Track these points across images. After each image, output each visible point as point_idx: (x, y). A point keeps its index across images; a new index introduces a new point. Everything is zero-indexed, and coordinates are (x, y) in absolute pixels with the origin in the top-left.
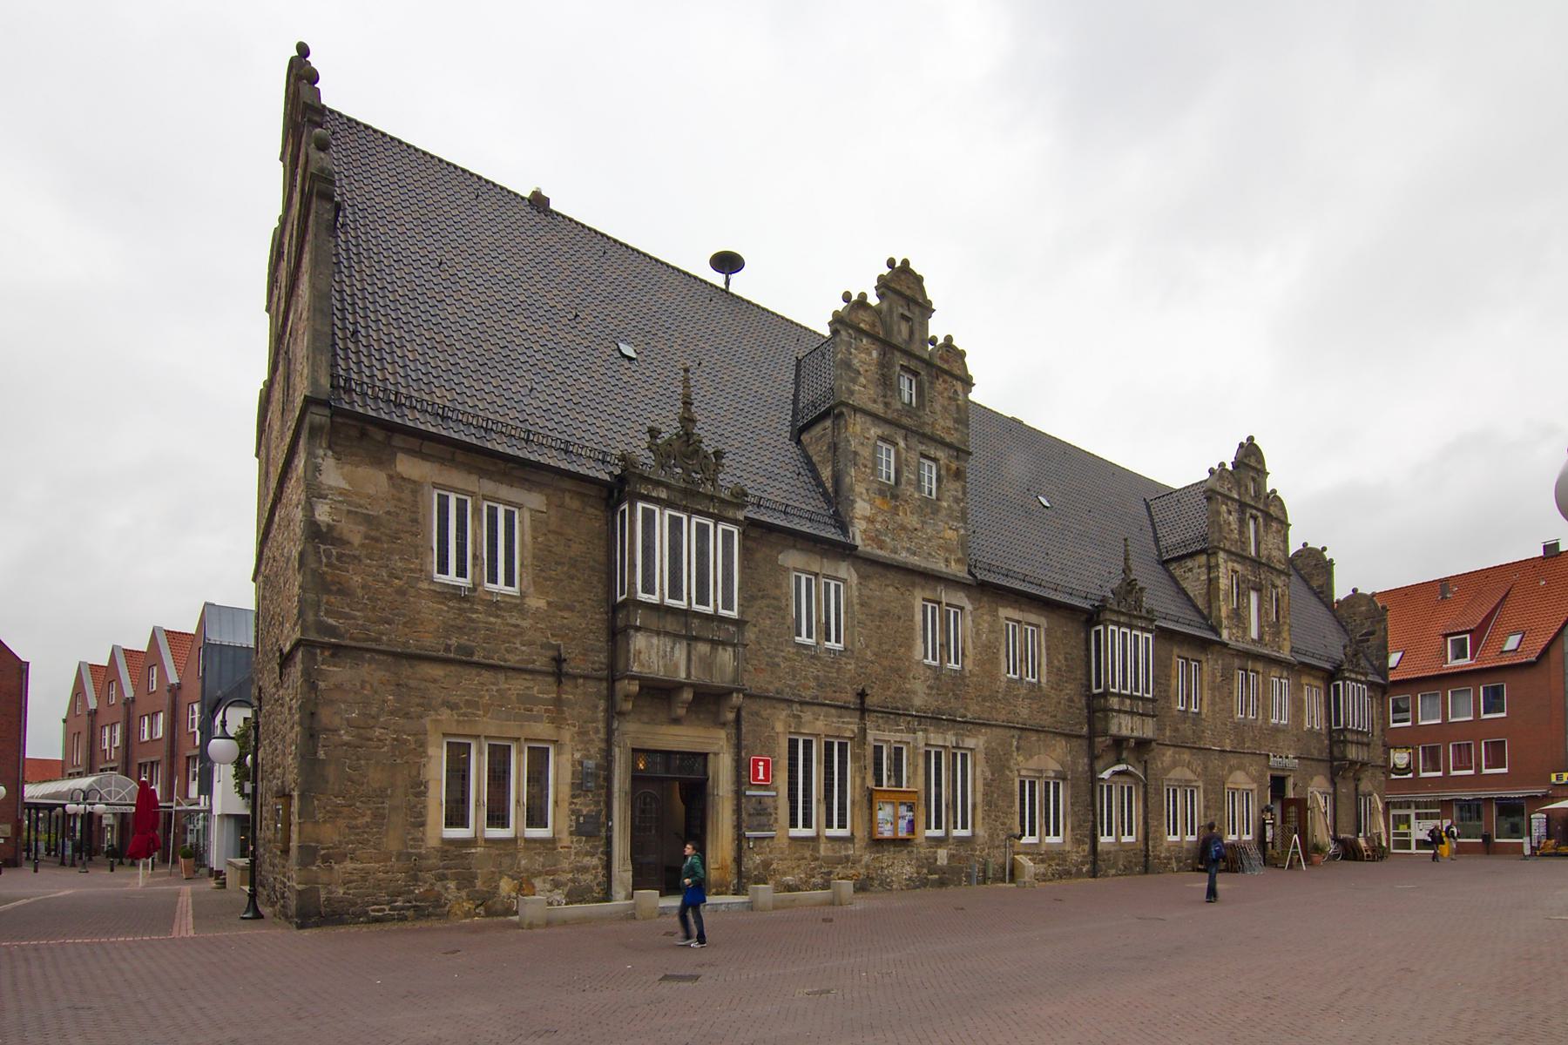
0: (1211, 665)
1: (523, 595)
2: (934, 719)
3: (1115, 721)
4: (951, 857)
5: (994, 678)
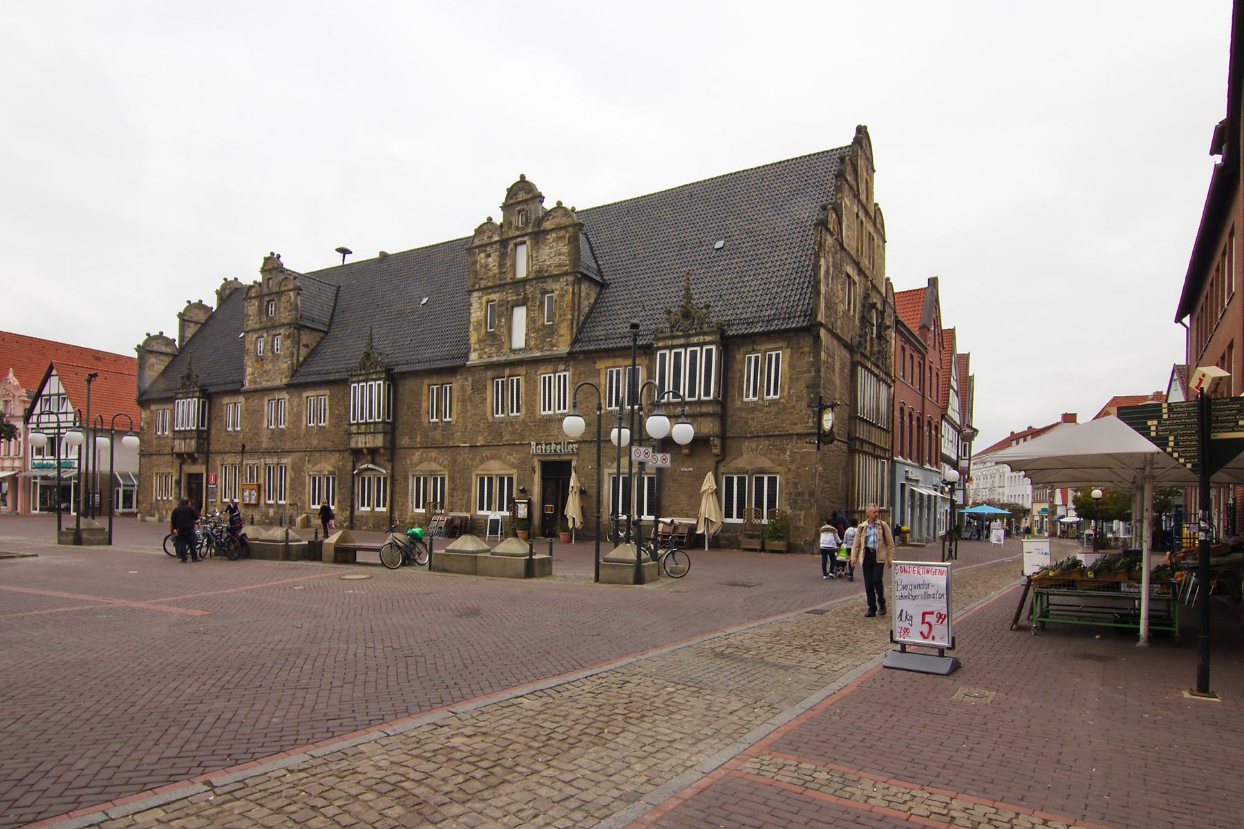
0: (457, 384)
2: (268, 453)
5: (299, 428)
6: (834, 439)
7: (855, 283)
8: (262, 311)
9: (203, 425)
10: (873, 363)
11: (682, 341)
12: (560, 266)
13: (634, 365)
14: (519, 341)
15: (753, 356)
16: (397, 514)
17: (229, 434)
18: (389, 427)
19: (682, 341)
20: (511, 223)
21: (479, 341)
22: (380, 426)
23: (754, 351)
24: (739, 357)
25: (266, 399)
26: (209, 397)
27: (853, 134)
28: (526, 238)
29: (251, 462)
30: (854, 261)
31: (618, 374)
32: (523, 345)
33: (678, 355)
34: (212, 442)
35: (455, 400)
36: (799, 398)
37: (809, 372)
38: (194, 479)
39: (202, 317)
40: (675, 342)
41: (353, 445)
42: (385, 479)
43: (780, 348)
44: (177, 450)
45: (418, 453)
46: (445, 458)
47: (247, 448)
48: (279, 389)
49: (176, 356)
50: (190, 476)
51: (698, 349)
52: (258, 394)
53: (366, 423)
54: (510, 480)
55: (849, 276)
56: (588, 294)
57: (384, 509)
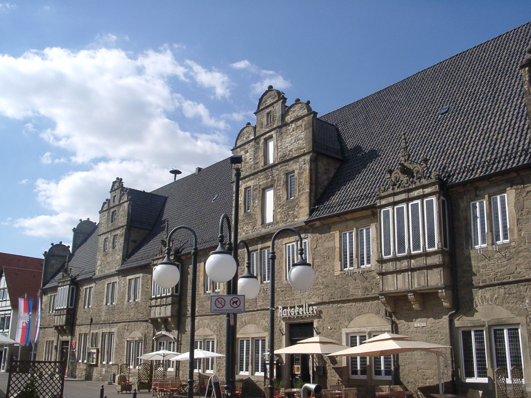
1: (510, 242)
3: (153, 312)
9: (71, 305)
11: (403, 196)
19: (403, 196)
22: (170, 299)
24: (462, 205)
28: (272, 133)
32: (272, 221)
40: (397, 198)
41: (152, 316)
47: (94, 321)
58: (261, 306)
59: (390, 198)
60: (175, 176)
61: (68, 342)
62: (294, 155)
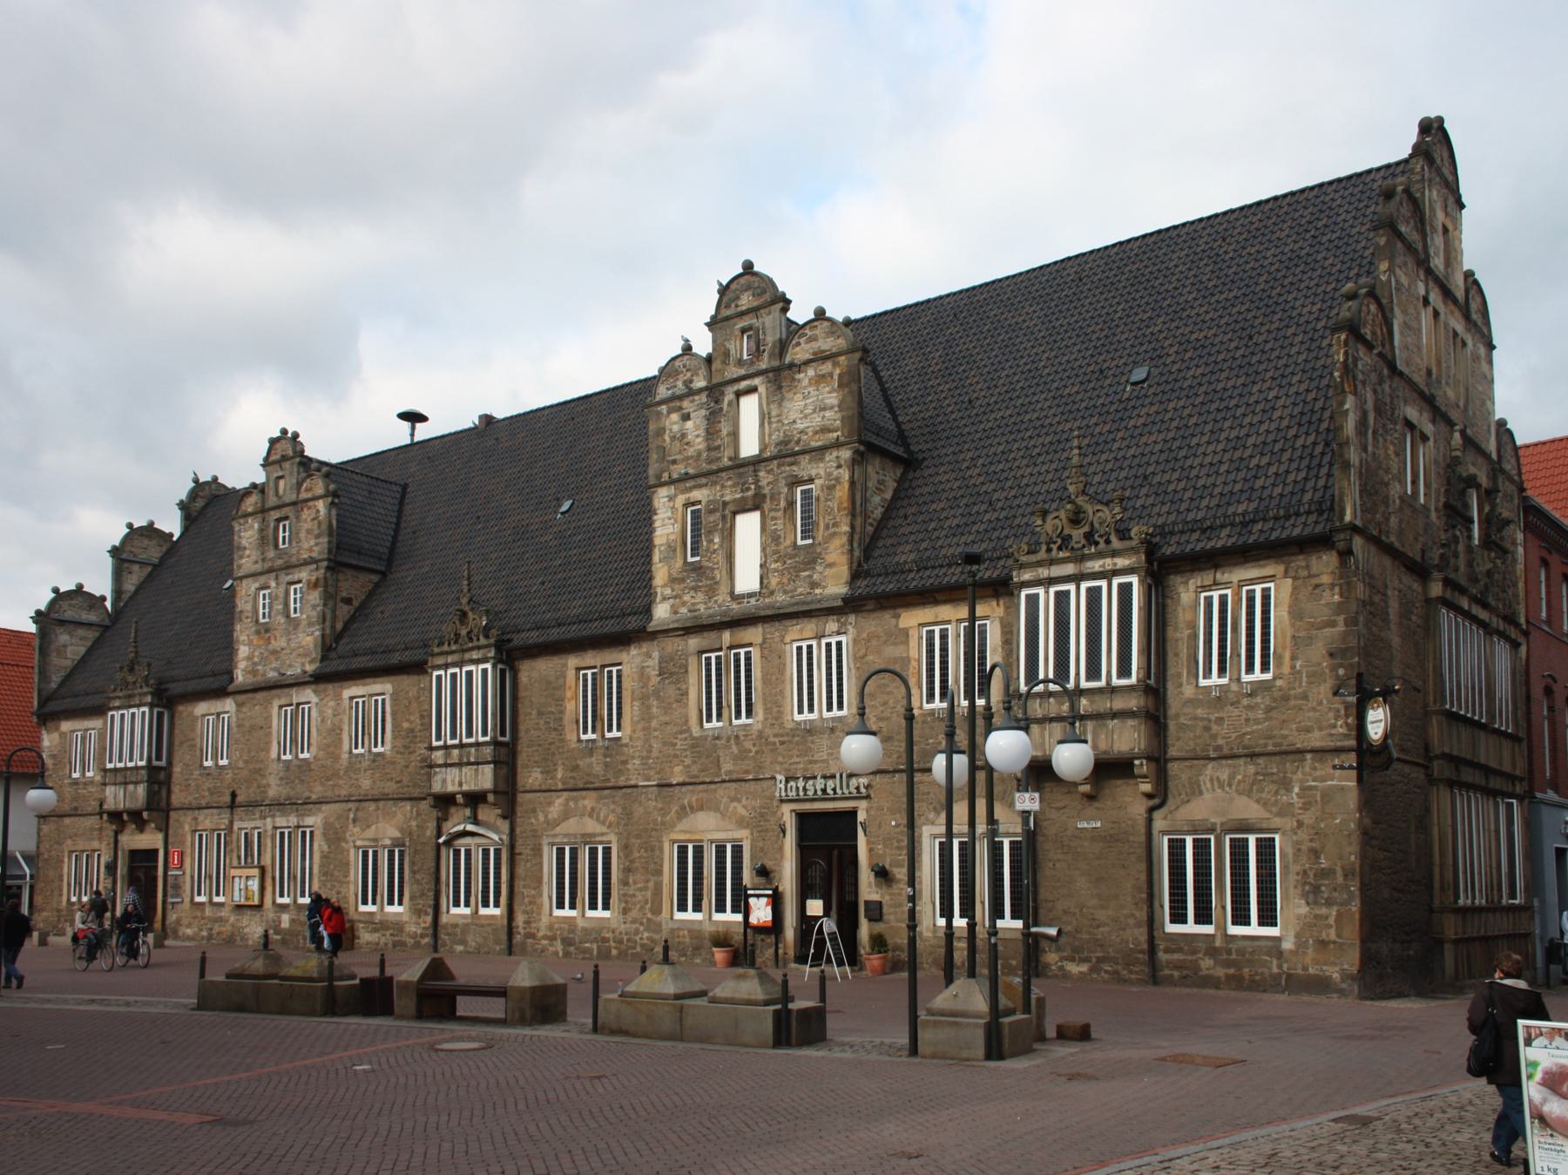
0: (633, 661)
1: (1274, 678)
2: (280, 805)
3: (438, 778)
4: (292, 921)
5: (337, 758)
6: (1390, 760)
7: (1424, 438)
8: (267, 539)
10: (1475, 600)
11: (1069, 569)
12: (824, 430)
13: (972, 618)
14: (747, 578)
15: (1216, 595)
16: (520, 919)
17: (207, 773)
18: (503, 750)
19: (1069, 569)
20: (727, 354)
21: (673, 580)
22: (488, 750)
23: (1216, 584)
25: (276, 703)
26: (167, 700)
27: (1411, 136)
28: (757, 381)
29: (248, 825)
30: (1421, 394)
31: (944, 637)
32: (754, 585)
33: (1062, 598)
34: (176, 789)
35: (626, 695)
36: (1316, 677)
37: (1333, 624)
38: (142, 862)
39: (154, 553)
40: (1056, 571)
41: (437, 787)
42: (498, 852)
43: (1271, 578)
44: (110, 805)
45: (558, 803)
46: (610, 809)
47: (239, 799)
48: (298, 684)
49: (106, 628)
50: (135, 854)
51: (1103, 583)
52: (260, 696)
53: (461, 746)
54: (738, 851)
55: (1410, 425)
56: (883, 480)
57: (497, 912)
58: (730, 772)
59: (1040, 570)
60: (413, 428)
61: (156, 851)
62: (814, 444)
